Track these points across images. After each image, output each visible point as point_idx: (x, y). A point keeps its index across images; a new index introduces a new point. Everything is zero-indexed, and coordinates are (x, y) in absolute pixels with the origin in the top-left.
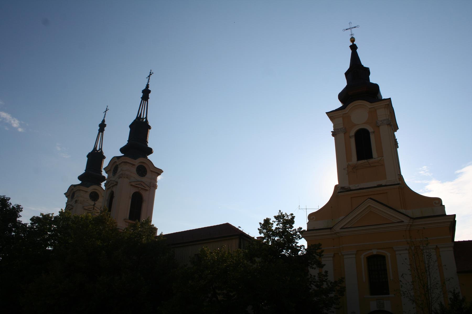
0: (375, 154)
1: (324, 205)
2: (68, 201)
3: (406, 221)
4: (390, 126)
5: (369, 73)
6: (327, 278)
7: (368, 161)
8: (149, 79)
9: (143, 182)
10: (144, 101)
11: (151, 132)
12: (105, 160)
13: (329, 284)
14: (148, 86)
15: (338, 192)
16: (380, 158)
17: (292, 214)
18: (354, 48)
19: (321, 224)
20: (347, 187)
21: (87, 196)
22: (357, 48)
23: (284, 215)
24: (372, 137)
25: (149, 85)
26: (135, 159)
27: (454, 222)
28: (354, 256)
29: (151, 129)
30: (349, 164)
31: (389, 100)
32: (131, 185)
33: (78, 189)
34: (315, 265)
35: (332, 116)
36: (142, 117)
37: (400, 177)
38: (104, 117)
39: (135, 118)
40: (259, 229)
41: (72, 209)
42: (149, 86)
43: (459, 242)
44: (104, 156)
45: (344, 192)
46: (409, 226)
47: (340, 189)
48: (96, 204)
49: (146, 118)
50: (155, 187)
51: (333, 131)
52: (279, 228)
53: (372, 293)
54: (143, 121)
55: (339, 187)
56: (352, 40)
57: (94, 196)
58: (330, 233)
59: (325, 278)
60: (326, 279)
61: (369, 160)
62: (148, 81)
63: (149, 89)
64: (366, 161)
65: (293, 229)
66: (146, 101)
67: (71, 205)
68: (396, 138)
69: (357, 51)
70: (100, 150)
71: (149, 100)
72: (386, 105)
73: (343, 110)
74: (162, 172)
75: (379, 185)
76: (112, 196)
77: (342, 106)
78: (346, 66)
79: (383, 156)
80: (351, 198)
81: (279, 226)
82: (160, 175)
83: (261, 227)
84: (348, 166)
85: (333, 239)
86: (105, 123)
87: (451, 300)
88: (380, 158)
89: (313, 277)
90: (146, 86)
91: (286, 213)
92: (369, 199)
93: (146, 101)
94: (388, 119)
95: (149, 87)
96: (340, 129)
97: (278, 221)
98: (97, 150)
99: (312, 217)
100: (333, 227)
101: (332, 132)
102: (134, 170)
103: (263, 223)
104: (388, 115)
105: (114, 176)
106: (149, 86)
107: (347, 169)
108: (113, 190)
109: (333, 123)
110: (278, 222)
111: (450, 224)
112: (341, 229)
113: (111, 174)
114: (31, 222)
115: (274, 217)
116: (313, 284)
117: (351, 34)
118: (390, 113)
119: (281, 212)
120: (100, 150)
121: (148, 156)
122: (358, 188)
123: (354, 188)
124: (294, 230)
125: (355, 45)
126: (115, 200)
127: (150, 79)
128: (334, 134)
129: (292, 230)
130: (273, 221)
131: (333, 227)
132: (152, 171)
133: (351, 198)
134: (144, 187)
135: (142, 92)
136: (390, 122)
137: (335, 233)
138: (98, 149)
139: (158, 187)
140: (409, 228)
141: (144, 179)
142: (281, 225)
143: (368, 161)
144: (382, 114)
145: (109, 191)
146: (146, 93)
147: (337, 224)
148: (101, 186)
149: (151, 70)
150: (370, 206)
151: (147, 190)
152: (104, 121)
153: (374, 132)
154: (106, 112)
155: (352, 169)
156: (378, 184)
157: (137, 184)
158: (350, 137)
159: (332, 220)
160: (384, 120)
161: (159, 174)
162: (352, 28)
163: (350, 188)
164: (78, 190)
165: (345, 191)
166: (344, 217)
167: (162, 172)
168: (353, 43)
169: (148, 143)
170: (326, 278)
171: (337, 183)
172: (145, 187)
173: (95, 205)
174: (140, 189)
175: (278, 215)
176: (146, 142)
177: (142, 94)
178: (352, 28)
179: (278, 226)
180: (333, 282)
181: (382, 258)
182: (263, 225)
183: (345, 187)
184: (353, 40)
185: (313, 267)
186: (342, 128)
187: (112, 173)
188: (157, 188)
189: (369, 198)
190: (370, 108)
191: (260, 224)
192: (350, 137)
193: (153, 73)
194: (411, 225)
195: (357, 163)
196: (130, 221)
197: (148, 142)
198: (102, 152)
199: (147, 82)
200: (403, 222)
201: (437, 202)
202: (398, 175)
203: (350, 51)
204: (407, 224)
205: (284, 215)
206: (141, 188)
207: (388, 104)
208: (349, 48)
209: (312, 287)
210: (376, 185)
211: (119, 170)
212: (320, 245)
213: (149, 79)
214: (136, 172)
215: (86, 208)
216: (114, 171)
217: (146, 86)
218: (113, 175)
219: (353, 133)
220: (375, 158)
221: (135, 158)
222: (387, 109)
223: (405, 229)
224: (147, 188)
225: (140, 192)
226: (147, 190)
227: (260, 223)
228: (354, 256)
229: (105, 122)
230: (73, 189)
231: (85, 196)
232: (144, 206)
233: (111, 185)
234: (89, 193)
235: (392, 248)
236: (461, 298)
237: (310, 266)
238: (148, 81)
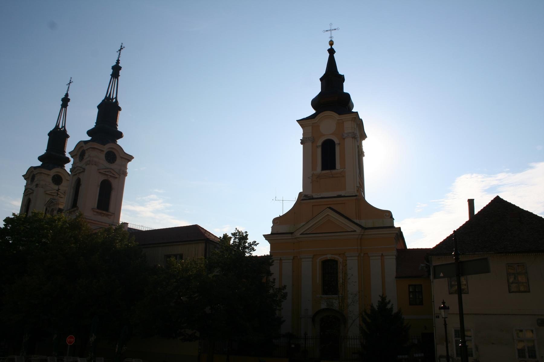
0: (338, 166)
1: (290, 209)
2: (26, 184)
3: (358, 230)
7: (331, 172)
8: (120, 54)
9: (112, 169)
10: (114, 79)
11: (121, 115)
12: (68, 139)
14: (118, 62)
16: (342, 170)
17: (246, 232)
18: (331, 52)
19: (283, 229)
20: (310, 195)
21: (49, 179)
22: (335, 52)
24: (337, 149)
25: (119, 60)
26: (104, 145)
28: (311, 260)
29: (121, 110)
30: (313, 173)
32: (100, 173)
33: (38, 172)
35: (302, 124)
36: (111, 97)
37: (358, 189)
38: (67, 90)
39: (103, 98)
41: (32, 193)
42: (119, 62)
43: (409, 249)
44: (68, 135)
46: (361, 235)
47: (303, 197)
48: (60, 189)
49: (64, 127)
50: (125, 174)
54: (113, 101)
55: (302, 195)
57: (57, 180)
58: (291, 237)
59: (272, 284)
62: (119, 56)
63: (120, 65)
64: (329, 171)
66: (116, 79)
67: (31, 189)
70: (63, 128)
71: (119, 78)
72: (353, 118)
73: (313, 120)
74: (133, 158)
75: (338, 195)
76: (78, 183)
77: (315, 112)
78: (322, 71)
79: (345, 168)
80: (313, 206)
82: (131, 161)
84: (312, 175)
86: (68, 97)
88: (342, 170)
90: (116, 61)
92: (328, 209)
93: (116, 79)
95: (119, 63)
96: (308, 138)
98: (59, 128)
99: (276, 222)
101: (301, 140)
102: (103, 156)
105: (80, 161)
106: (119, 62)
107: (311, 178)
108: (80, 177)
111: (395, 235)
113: (78, 159)
114: (4, 223)
119: (237, 229)
120: (63, 128)
121: (117, 141)
122: (320, 197)
123: (316, 197)
126: (81, 188)
127: (121, 54)
128: (302, 142)
132: (122, 158)
134: (113, 174)
135: (112, 69)
138: (60, 127)
139: (128, 174)
141: (113, 166)
143: (331, 172)
144: (348, 126)
145: (75, 178)
146: (116, 70)
147: (316, 216)
148: (65, 168)
149: (122, 44)
150: (328, 215)
151: (116, 178)
152: (67, 95)
153: (339, 144)
154: (69, 84)
156: (338, 194)
157: (105, 172)
158: (317, 147)
159: (294, 225)
160: (350, 133)
161: (129, 161)
162: (332, 30)
163: (312, 196)
164: (38, 173)
165: (308, 199)
167: (133, 158)
168: (331, 47)
169: (117, 126)
170: (273, 284)
171: (302, 191)
172: (115, 175)
173: (59, 191)
174: (109, 176)
176: (115, 125)
177: (112, 70)
178: (332, 30)
181: (334, 262)
184: (331, 43)
187: (78, 158)
188: (127, 175)
189: (328, 208)
190: (338, 120)
192: (317, 147)
193: (124, 47)
194: (362, 235)
196: (98, 211)
197: (118, 125)
198: (65, 130)
199: (118, 57)
200: (355, 231)
201: (388, 214)
202: (357, 187)
203: (328, 55)
204: (359, 233)
206: (111, 176)
208: (327, 52)
210: (336, 196)
211: (87, 155)
213: (120, 54)
214: (104, 158)
215: (48, 192)
216: (80, 155)
217: (116, 61)
218: (79, 160)
219: (320, 143)
220: (337, 170)
221: (104, 144)
224: (117, 176)
225: (109, 179)
226: (116, 178)
228: (311, 260)
229: (68, 96)
230: (33, 171)
231: (46, 179)
232: (113, 194)
233: (77, 172)
234: (51, 177)
238: (119, 56)
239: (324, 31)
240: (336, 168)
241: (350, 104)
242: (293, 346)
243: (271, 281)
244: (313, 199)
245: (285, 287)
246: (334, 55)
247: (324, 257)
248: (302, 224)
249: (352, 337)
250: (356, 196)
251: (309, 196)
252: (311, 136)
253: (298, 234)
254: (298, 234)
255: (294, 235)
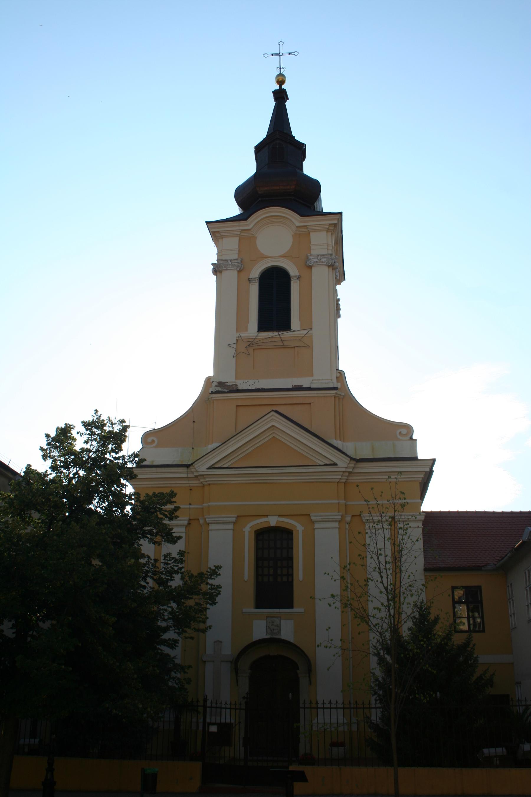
0: (295, 322)
3: (343, 463)
4: (333, 269)
5: (303, 155)
6: (183, 565)
13: (187, 578)
15: (212, 392)
16: (305, 332)
17: (123, 421)
20: (231, 384)
23: (104, 420)
27: (429, 474)
28: (231, 526)
30: (240, 336)
31: (340, 215)
34: (158, 536)
35: (218, 232)
37: (339, 374)
40: (42, 449)
45: (224, 392)
46: (347, 474)
47: (216, 386)
51: (216, 262)
52: (89, 451)
53: (259, 604)
56: (280, 80)
58: (185, 475)
59: (178, 566)
60: (181, 569)
61: (281, 332)
64: (276, 333)
65: (120, 454)
68: (338, 298)
69: (287, 104)
72: (330, 224)
73: (242, 223)
75: (296, 385)
79: (311, 329)
80: (237, 406)
81: (91, 445)
83: (49, 444)
84: (237, 340)
85: (191, 489)
87: (414, 621)
88: (305, 332)
89: (152, 561)
91: (109, 417)
94: (331, 255)
96: (231, 261)
97: (89, 434)
99: (150, 440)
100: (194, 463)
101: (213, 264)
103: (53, 434)
104: (332, 247)
107: (235, 346)
109: (217, 246)
110: (88, 436)
112: (208, 469)
115: (82, 422)
116: (151, 577)
117: (279, 66)
118: (336, 243)
119: (99, 413)
122: (253, 387)
123: (245, 387)
124: (121, 457)
125: (284, 91)
128: (217, 270)
129: (117, 456)
130: (78, 433)
131: (194, 464)
133: (237, 406)
136: (333, 261)
137: (196, 477)
140: (346, 478)
142: (94, 443)
143: (279, 335)
153: (299, 277)
155: (246, 347)
158: (250, 281)
159: (193, 448)
160: (324, 255)
162: (284, 54)
166: (217, 445)
171: (211, 373)
175: (91, 420)
178: (284, 54)
179: (89, 444)
180: (195, 574)
182: (53, 439)
183: (227, 383)
184: (281, 81)
185: (157, 540)
186: (235, 260)
190: (297, 227)
191: (46, 436)
192: (250, 281)
194: (350, 473)
195: (257, 336)
200: (335, 464)
201: (404, 431)
203: (272, 103)
204: (344, 470)
205: (105, 422)
207: (335, 225)
208: (272, 95)
209: (148, 583)
210: (291, 387)
212: (173, 494)
219: (256, 272)
220: (294, 331)
222: (332, 234)
223: (338, 480)
227: (48, 436)
228: (231, 526)
235: (309, 515)
236: (432, 617)
237: (148, 538)
239: (266, 55)
240: (291, 329)
241: (318, 203)
242: (213, 729)
243: (173, 558)
244: (238, 391)
245: (215, 572)
246: (286, 104)
247: (260, 523)
248: (211, 447)
249: (350, 703)
250: (335, 389)
251: (229, 386)
252: (236, 257)
253: (202, 468)
254: (202, 468)
255: (193, 470)
